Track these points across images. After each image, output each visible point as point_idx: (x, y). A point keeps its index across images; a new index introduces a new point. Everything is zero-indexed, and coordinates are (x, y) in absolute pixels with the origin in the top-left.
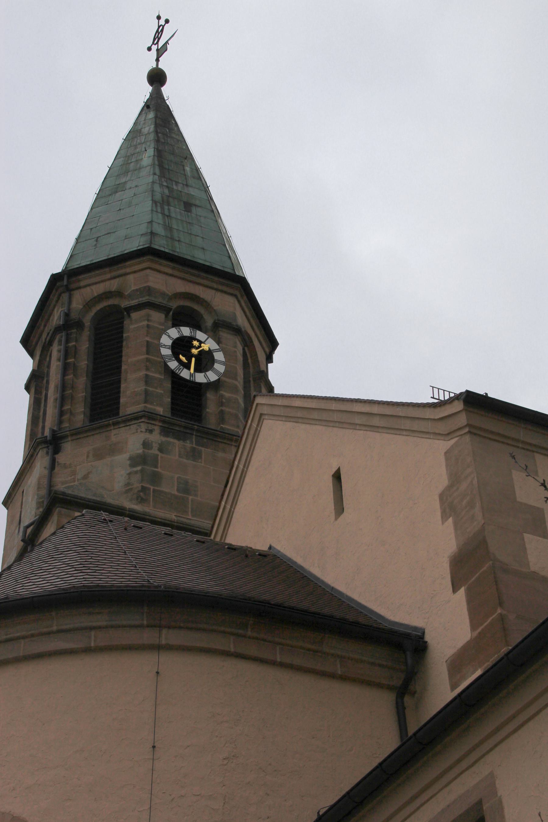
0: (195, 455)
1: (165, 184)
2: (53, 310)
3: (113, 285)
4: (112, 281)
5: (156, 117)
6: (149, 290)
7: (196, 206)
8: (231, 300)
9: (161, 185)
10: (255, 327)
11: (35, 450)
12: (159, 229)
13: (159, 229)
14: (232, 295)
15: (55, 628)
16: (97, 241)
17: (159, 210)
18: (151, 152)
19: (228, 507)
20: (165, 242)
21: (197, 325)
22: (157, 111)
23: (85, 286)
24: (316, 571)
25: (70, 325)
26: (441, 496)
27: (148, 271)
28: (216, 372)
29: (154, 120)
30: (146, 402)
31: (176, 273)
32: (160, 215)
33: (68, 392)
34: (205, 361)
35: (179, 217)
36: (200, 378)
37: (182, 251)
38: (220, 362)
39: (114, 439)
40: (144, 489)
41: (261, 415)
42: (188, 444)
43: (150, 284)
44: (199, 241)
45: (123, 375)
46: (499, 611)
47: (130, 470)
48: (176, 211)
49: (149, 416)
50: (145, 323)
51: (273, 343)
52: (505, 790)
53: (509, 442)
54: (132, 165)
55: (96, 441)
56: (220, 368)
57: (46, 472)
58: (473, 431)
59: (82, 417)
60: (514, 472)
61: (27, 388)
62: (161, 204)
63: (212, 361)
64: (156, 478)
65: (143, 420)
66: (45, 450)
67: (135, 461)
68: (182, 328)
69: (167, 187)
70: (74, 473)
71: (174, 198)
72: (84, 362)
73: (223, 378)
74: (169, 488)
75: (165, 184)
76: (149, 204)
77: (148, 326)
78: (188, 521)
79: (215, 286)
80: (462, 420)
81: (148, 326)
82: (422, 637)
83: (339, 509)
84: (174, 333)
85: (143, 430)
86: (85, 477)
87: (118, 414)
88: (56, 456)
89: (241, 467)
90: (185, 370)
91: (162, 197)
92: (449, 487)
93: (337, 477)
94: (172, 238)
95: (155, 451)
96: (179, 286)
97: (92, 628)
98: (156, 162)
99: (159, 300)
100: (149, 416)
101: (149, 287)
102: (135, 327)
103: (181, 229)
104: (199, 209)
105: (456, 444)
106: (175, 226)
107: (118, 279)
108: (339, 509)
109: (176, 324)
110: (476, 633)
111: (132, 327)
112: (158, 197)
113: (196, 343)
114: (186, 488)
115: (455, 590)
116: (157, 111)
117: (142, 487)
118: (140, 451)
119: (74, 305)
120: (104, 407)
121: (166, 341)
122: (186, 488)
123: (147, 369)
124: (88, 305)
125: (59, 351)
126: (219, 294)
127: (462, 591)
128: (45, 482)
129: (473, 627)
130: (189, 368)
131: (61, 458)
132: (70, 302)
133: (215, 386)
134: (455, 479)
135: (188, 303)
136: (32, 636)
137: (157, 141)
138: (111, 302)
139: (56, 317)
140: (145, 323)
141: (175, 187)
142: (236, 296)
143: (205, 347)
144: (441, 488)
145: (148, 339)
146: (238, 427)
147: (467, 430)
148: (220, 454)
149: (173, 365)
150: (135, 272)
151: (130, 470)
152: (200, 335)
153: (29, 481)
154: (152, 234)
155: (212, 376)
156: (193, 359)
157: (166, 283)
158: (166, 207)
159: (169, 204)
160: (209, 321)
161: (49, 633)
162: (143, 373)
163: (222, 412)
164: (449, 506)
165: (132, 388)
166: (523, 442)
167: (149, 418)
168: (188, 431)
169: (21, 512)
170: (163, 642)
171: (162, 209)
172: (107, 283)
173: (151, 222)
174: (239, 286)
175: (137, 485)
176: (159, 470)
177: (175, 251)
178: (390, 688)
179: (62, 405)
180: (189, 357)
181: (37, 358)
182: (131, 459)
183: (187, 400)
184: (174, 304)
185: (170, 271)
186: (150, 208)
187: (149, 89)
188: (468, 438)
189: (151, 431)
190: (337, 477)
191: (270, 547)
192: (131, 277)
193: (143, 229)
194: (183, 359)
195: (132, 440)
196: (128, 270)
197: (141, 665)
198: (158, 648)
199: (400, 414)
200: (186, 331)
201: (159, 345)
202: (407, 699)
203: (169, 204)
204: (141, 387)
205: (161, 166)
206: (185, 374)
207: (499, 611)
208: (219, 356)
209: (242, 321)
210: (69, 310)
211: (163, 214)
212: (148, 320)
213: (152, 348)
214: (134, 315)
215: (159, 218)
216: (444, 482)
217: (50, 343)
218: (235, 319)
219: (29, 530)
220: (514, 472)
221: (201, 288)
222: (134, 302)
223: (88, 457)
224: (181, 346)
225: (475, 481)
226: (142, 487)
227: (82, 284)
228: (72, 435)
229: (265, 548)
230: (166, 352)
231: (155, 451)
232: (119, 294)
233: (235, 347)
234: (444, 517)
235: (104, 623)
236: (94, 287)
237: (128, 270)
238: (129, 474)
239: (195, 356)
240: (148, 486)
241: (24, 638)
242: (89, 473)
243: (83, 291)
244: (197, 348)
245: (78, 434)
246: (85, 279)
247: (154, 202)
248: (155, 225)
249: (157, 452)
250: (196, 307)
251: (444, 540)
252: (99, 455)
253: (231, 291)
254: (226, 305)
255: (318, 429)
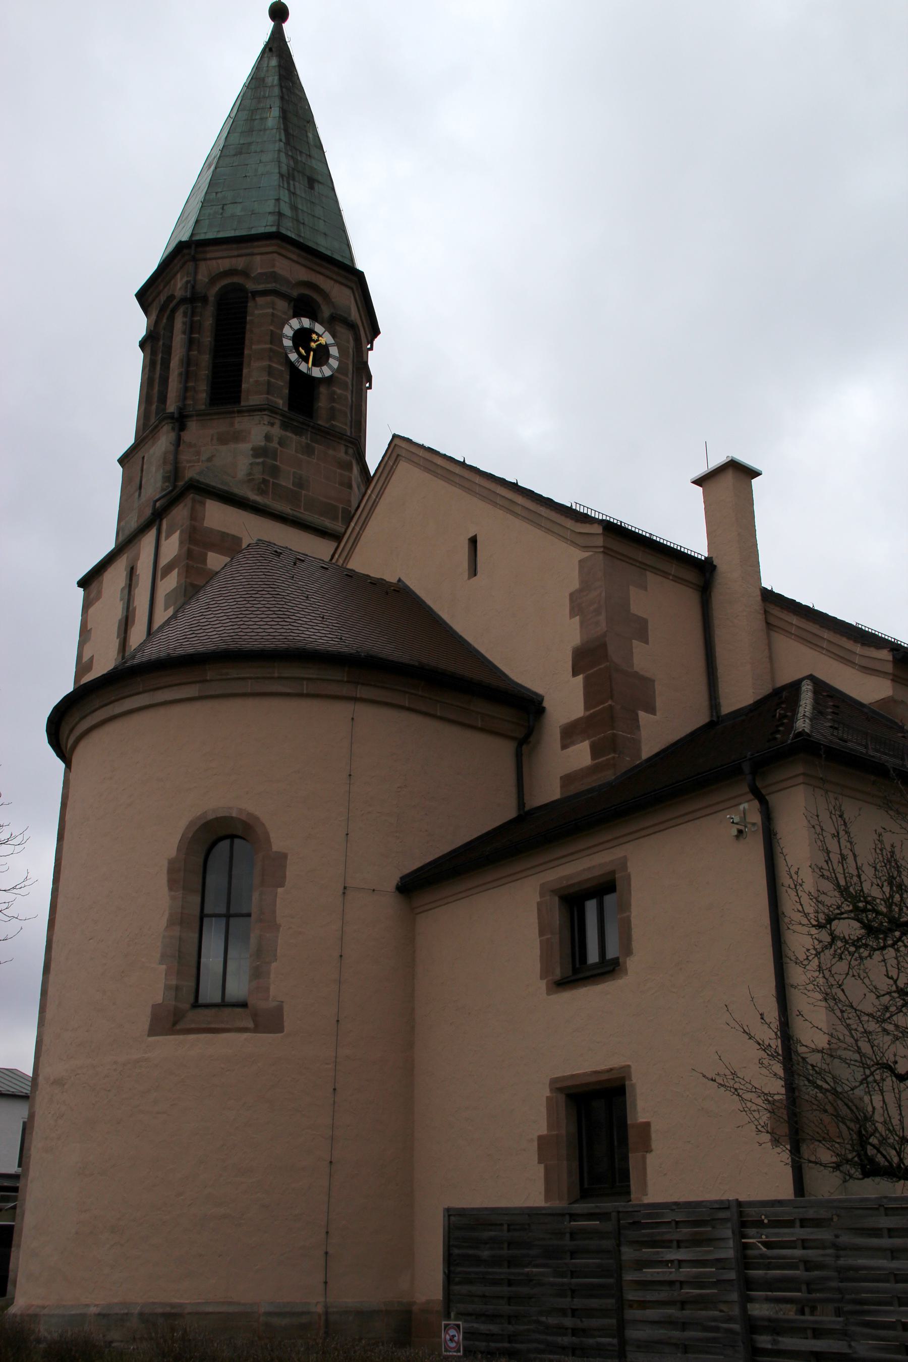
0: (308, 450)
1: (290, 153)
2: (175, 275)
3: (240, 263)
4: (239, 259)
5: (280, 66)
6: (274, 276)
7: (319, 182)
8: (348, 292)
9: (287, 154)
10: (363, 318)
11: (160, 423)
12: (286, 210)
13: (286, 210)
14: (346, 286)
15: (276, 675)
16: (223, 209)
17: (286, 186)
18: (276, 112)
19: (357, 529)
20: (291, 224)
21: (314, 318)
22: (277, 48)
23: (211, 259)
24: (445, 616)
25: (194, 299)
26: (571, 595)
27: (275, 255)
28: (330, 367)
29: (277, 69)
30: (268, 393)
31: (301, 260)
32: (286, 192)
33: (193, 368)
34: (322, 356)
35: (303, 195)
36: (316, 372)
37: (307, 237)
38: (335, 357)
39: (237, 426)
40: (265, 481)
41: (398, 455)
42: (304, 440)
43: (276, 269)
44: (321, 226)
45: (246, 360)
46: (610, 702)
47: (252, 460)
48: (300, 187)
49: (272, 410)
50: (270, 311)
51: (375, 331)
52: (632, 868)
53: (631, 561)
54: (256, 122)
55: (219, 426)
56: (334, 363)
57: (172, 448)
58: (607, 551)
59: (204, 395)
60: (631, 588)
61: (143, 345)
62: (287, 177)
63: (328, 355)
64: (275, 471)
65: (266, 413)
66: (171, 425)
67: (258, 452)
68: (303, 319)
69: (292, 157)
70: (198, 453)
71: (299, 172)
72: (207, 339)
73: (337, 374)
74: (286, 482)
75: (290, 153)
76: (276, 177)
77: (273, 315)
78: (299, 515)
79: (335, 277)
80: (600, 541)
81: (273, 315)
82: (543, 700)
83: (473, 571)
84: (295, 323)
85: (266, 423)
86: (210, 459)
87: (239, 402)
88: (182, 433)
89: (374, 497)
90: (303, 363)
91: (288, 170)
92: (580, 591)
93: (473, 541)
94: (298, 221)
95: (275, 445)
96: (303, 274)
97: (304, 679)
98: (282, 126)
99: (284, 289)
100: (272, 410)
101: (274, 272)
102: (259, 312)
103: (305, 209)
104: (320, 186)
105: (591, 556)
106: (300, 206)
107: (244, 258)
108: (473, 571)
109: (297, 315)
110: (588, 713)
111: (256, 312)
112: (284, 170)
113: (314, 336)
114: (300, 483)
115: (575, 674)
116: (277, 48)
117: (264, 479)
118: (263, 444)
119: (200, 277)
120: (226, 392)
121: (288, 331)
122: (300, 483)
123: (270, 359)
124: (213, 280)
125: (184, 323)
126: (337, 286)
127: (580, 678)
128: (171, 457)
129: (587, 708)
130: (307, 362)
131: (187, 436)
132: (196, 273)
133: (329, 381)
134: (586, 585)
135: (307, 292)
136: (258, 678)
137: (282, 98)
138: (236, 279)
139: (179, 285)
140: (270, 311)
141: (299, 159)
142: (352, 289)
143: (323, 341)
144: (572, 589)
145: (272, 328)
146: (346, 424)
147: (602, 550)
148: (331, 452)
149: (293, 357)
150: (262, 254)
151: (252, 460)
152: (319, 328)
153: (152, 451)
154: (280, 214)
155: (327, 372)
156: (312, 353)
157: (292, 270)
158: (291, 182)
159: (294, 180)
160: (326, 312)
161: (273, 678)
162: (266, 363)
163: (332, 409)
164: (577, 605)
165: (255, 375)
166: (640, 562)
167: (272, 411)
168: (305, 427)
169: (141, 477)
170: (358, 696)
171: (288, 183)
172: (234, 260)
173: (278, 200)
174: (356, 279)
175: (258, 476)
176: (278, 463)
177: (300, 236)
178: (512, 738)
179: (186, 381)
180: (308, 350)
181: (154, 317)
182: (253, 449)
183: (303, 390)
184: (295, 293)
185: (294, 257)
186: (276, 183)
187: (270, 25)
188: (601, 556)
189: (272, 424)
190: (473, 541)
191: (400, 580)
192: (258, 258)
193: (270, 206)
194: (303, 352)
195: (257, 431)
196: (256, 251)
197: (340, 711)
198: (355, 699)
199: (543, 514)
200: (306, 322)
201: (281, 336)
202: (525, 748)
203: (294, 180)
204: (264, 378)
205: (286, 130)
206: (303, 367)
207: (610, 702)
208: (334, 351)
209: (354, 315)
210: (195, 280)
211: (289, 190)
212: (273, 309)
213: (276, 338)
214: (260, 300)
215: (285, 196)
216: (575, 585)
217: (174, 311)
218: (350, 315)
219: (158, 504)
220: (631, 588)
221: (321, 277)
222: (261, 287)
223: (212, 439)
224: (302, 337)
225: (603, 594)
226: (264, 479)
227: (208, 256)
228: (197, 416)
229: (394, 580)
230: (288, 343)
231: (275, 445)
232: (245, 273)
233: (348, 342)
234: (572, 615)
235: (315, 676)
236: (220, 261)
237: (256, 251)
238: (251, 464)
239: (314, 350)
240: (267, 478)
241: (250, 678)
242: (213, 456)
243: (209, 262)
244: (315, 342)
245: (202, 415)
246: (212, 252)
247: (282, 176)
248: (282, 203)
249: (277, 446)
250: (315, 296)
251: (570, 634)
252: (223, 440)
253: (349, 284)
254: (342, 296)
255: (457, 491)
